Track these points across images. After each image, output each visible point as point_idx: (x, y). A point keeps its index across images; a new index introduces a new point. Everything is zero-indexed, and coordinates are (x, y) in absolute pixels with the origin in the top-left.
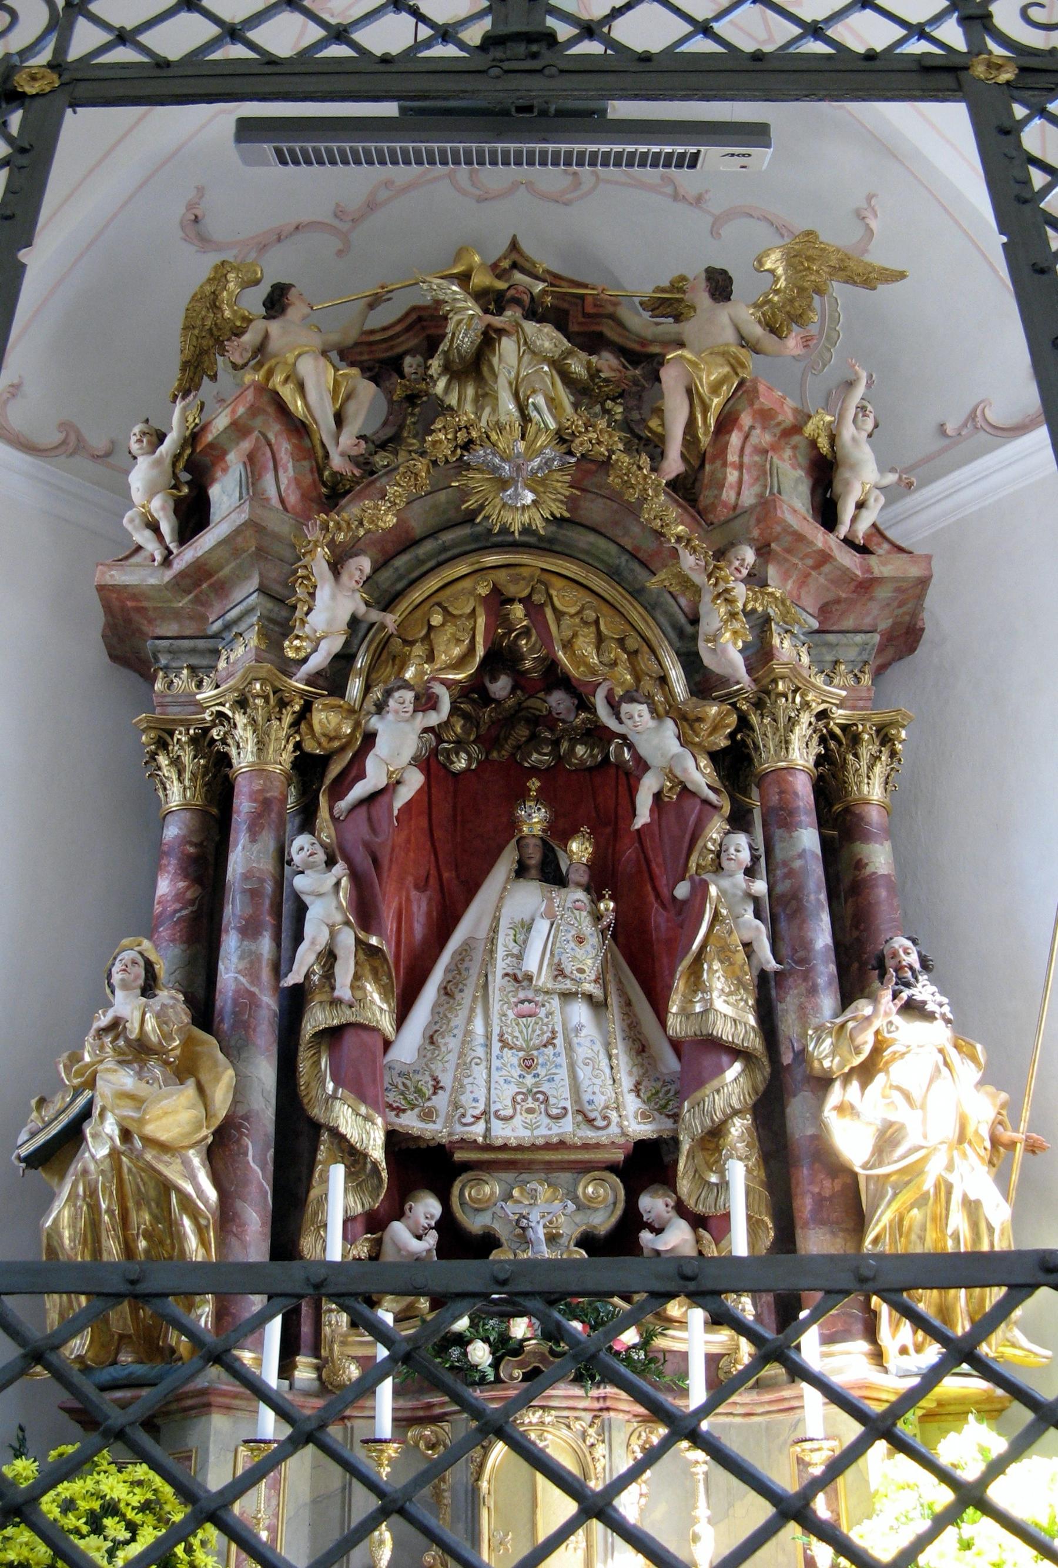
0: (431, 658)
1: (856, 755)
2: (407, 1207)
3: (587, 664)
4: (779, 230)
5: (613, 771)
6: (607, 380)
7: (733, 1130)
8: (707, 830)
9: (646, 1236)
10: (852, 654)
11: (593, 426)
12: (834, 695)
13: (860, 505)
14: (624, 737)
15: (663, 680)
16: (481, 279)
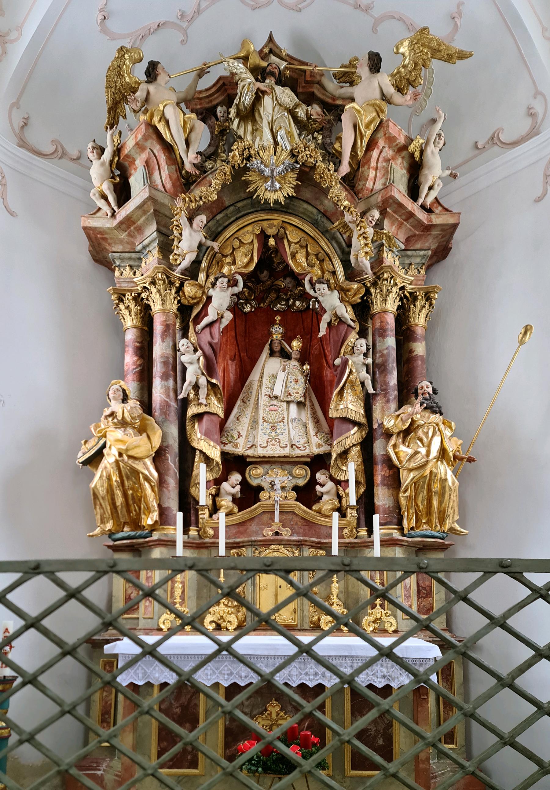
0: (234, 263)
1: (415, 305)
3: (301, 266)
4: (409, 26)
5: (311, 312)
6: (315, 121)
9: (318, 488)
10: (418, 260)
12: (407, 279)
13: (431, 188)
14: (316, 298)
15: (334, 273)
16: (255, 60)
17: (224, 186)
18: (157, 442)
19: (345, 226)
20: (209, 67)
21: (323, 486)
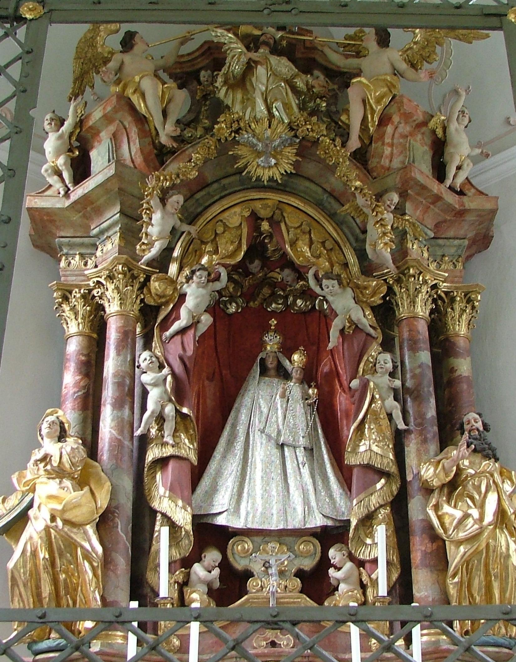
0: (216, 252)
1: (452, 309)
2: (203, 555)
3: (304, 257)
5: (318, 314)
7: (380, 515)
8: (369, 350)
9: (331, 571)
10: (453, 250)
11: (310, 121)
12: (441, 276)
13: (459, 168)
14: (324, 297)
15: (346, 265)
17: (206, 161)
18: (103, 501)
19: (358, 209)
20: (194, 34)
21: (339, 569)
